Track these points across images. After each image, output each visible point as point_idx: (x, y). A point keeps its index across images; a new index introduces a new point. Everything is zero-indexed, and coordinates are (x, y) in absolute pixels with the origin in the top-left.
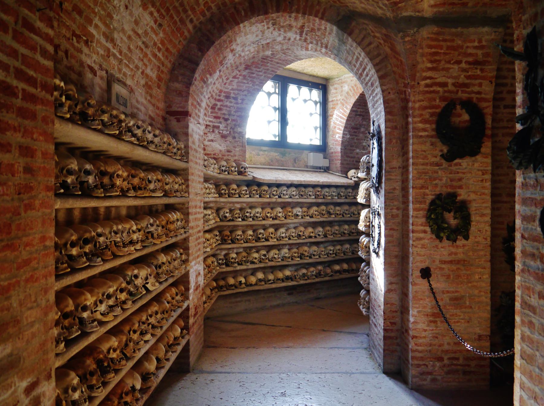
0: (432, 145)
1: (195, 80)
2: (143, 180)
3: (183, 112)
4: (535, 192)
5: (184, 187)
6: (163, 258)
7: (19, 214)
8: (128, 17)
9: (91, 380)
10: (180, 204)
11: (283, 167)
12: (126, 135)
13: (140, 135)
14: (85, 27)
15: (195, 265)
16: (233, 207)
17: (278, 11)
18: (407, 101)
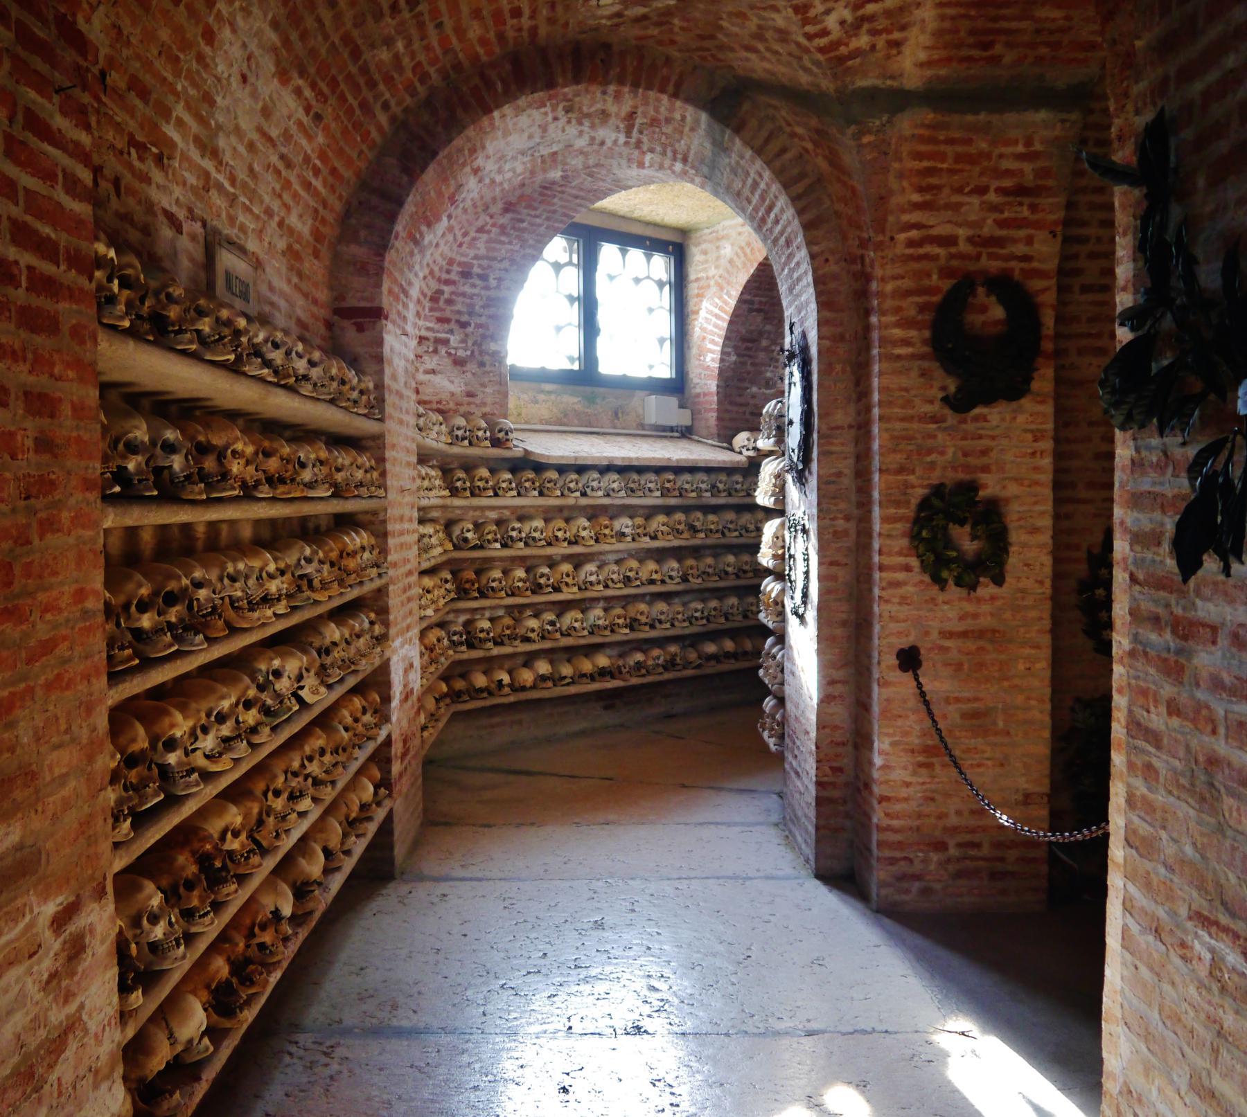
0: (922, 375)
1: (396, 238)
2: (288, 462)
3: (371, 309)
4: (1162, 479)
5: (375, 474)
6: (333, 633)
7: (28, 542)
8: (248, 102)
9: (189, 898)
10: (366, 513)
11: (589, 428)
12: (250, 364)
13: (279, 362)
14: (156, 125)
15: (402, 646)
16: (481, 517)
17: (577, 80)
18: (868, 278)
